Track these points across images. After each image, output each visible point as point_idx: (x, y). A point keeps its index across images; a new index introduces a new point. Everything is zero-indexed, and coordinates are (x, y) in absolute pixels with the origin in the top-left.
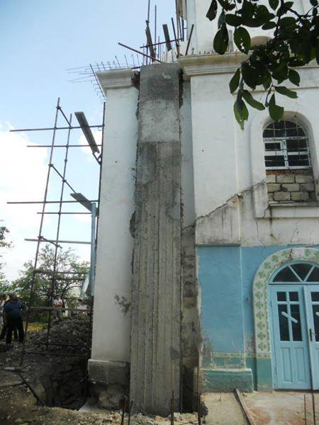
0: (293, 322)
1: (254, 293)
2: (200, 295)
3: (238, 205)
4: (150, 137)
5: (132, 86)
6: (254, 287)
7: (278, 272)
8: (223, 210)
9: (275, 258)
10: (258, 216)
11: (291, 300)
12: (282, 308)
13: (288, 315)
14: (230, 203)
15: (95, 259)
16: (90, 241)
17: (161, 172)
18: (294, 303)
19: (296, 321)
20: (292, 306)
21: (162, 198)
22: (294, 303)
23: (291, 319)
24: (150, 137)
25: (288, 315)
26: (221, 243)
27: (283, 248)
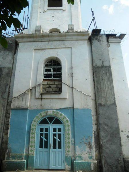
7: (42, 119)
8: (23, 95)
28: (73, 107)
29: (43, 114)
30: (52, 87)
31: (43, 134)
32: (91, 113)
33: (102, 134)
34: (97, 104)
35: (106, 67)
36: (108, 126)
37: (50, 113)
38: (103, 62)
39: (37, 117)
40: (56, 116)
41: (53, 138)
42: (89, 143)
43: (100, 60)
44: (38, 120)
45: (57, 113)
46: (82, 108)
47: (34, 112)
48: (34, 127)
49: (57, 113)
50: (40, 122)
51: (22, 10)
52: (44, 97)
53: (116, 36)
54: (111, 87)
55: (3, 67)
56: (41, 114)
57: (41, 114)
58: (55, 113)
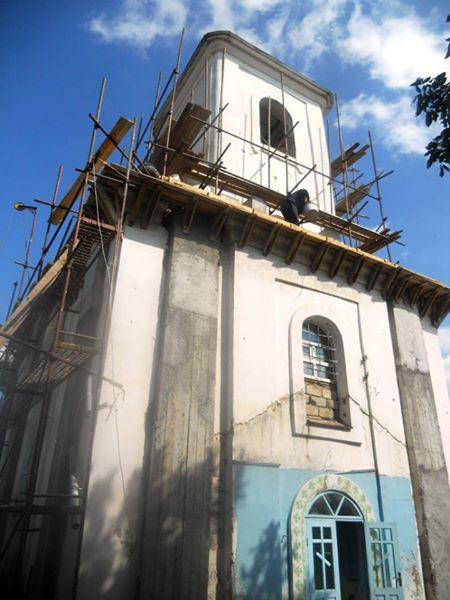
0: (326, 565)
1: (292, 528)
2: (235, 531)
3: (277, 414)
4: (184, 303)
5: (106, 379)
6: (292, 520)
7: (314, 501)
8: (263, 418)
9: (311, 486)
10: (297, 432)
11: (325, 538)
12: (317, 547)
13: (322, 556)
14: (270, 411)
15: (34, 460)
16: (158, 253)
17: (195, 353)
18: (317, 541)
19: (318, 554)
20: (325, 544)
21: (194, 390)
22: (317, 541)
23: (325, 561)
24: (184, 303)
25: (322, 556)
26: (260, 461)
27: (318, 473)
29: (319, 486)
33: (433, 545)
35: (423, 374)
37: (333, 483)
38: (417, 359)
39: (304, 494)
41: (332, 564)
42: (414, 567)
43: (412, 353)
44: (306, 503)
45: (348, 483)
47: (303, 474)
48: (297, 525)
50: (324, 513)
52: (316, 431)
53: (362, 243)
54: (55, 336)
57: (311, 486)
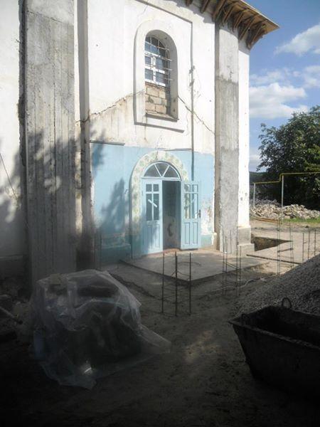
7: (150, 167)
8: (112, 110)
28: (193, 150)
29: (152, 158)
30: (155, 102)
31: (151, 195)
32: (73, 174)
34: (27, 137)
35: (234, 83)
36: (229, 183)
37: (162, 156)
40: (170, 164)
45: (172, 156)
46: (204, 152)
47: (139, 151)
49: (172, 156)
51: (203, 19)
55: (52, 15)
56: (147, 158)
57: (147, 158)
58: (169, 158)
